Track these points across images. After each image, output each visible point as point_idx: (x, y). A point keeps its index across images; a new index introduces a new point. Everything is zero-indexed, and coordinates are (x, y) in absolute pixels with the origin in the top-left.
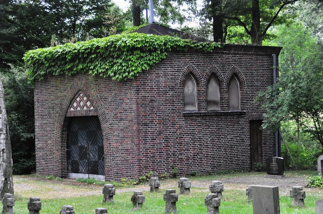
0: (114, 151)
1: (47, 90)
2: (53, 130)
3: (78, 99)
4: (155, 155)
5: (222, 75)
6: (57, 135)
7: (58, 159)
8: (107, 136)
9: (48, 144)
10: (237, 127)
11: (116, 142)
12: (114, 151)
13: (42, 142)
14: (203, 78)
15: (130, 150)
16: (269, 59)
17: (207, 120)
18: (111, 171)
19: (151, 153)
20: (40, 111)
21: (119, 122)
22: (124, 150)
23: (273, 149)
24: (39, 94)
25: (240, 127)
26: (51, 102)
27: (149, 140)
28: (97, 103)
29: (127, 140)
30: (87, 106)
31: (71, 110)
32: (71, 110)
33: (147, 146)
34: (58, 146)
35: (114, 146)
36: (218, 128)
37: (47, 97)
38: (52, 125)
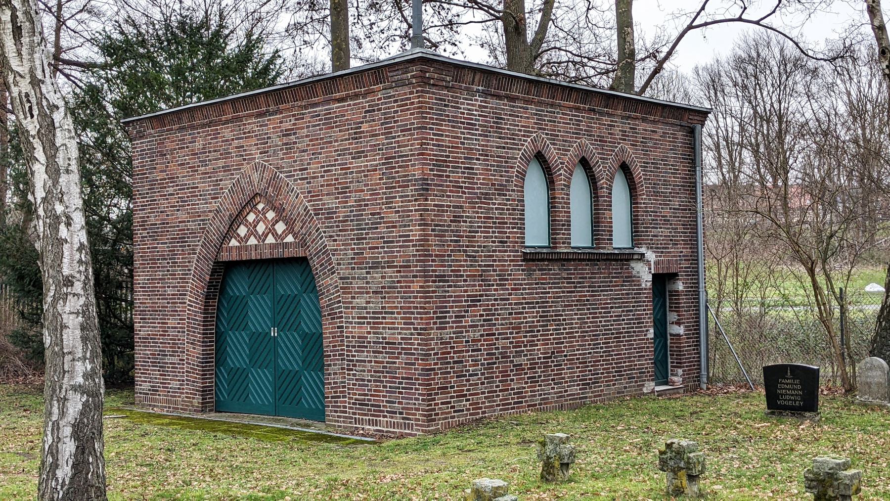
0: (354, 347)
1: (167, 199)
2: (180, 295)
3: (251, 217)
4: (463, 357)
5: (600, 166)
6: (191, 306)
7: (194, 365)
8: (333, 309)
9: (168, 327)
10: (629, 290)
11: (359, 323)
12: (354, 347)
13: (151, 323)
14: (562, 167)
15: (400, 344)
16: (687, 136)
17: (571, 270)
18: (344, 397)
19: (455, 353)
20: (148, 248)
21: (368, 273)
22: (382, 343)
23: (693, 342)
24: (147, 209)
25: (633, 290)
26: (178, 226)
27: (451, 317)
28: (304, 224)
29: (391, 318)
30: (275, 235)
31: (231, 245)
32: (231, 245)
33: (448, 334)
34: (194, 332)
35: (352, 332)
36: (593, 291)
37: (168, 215)
38: (179, 283)
